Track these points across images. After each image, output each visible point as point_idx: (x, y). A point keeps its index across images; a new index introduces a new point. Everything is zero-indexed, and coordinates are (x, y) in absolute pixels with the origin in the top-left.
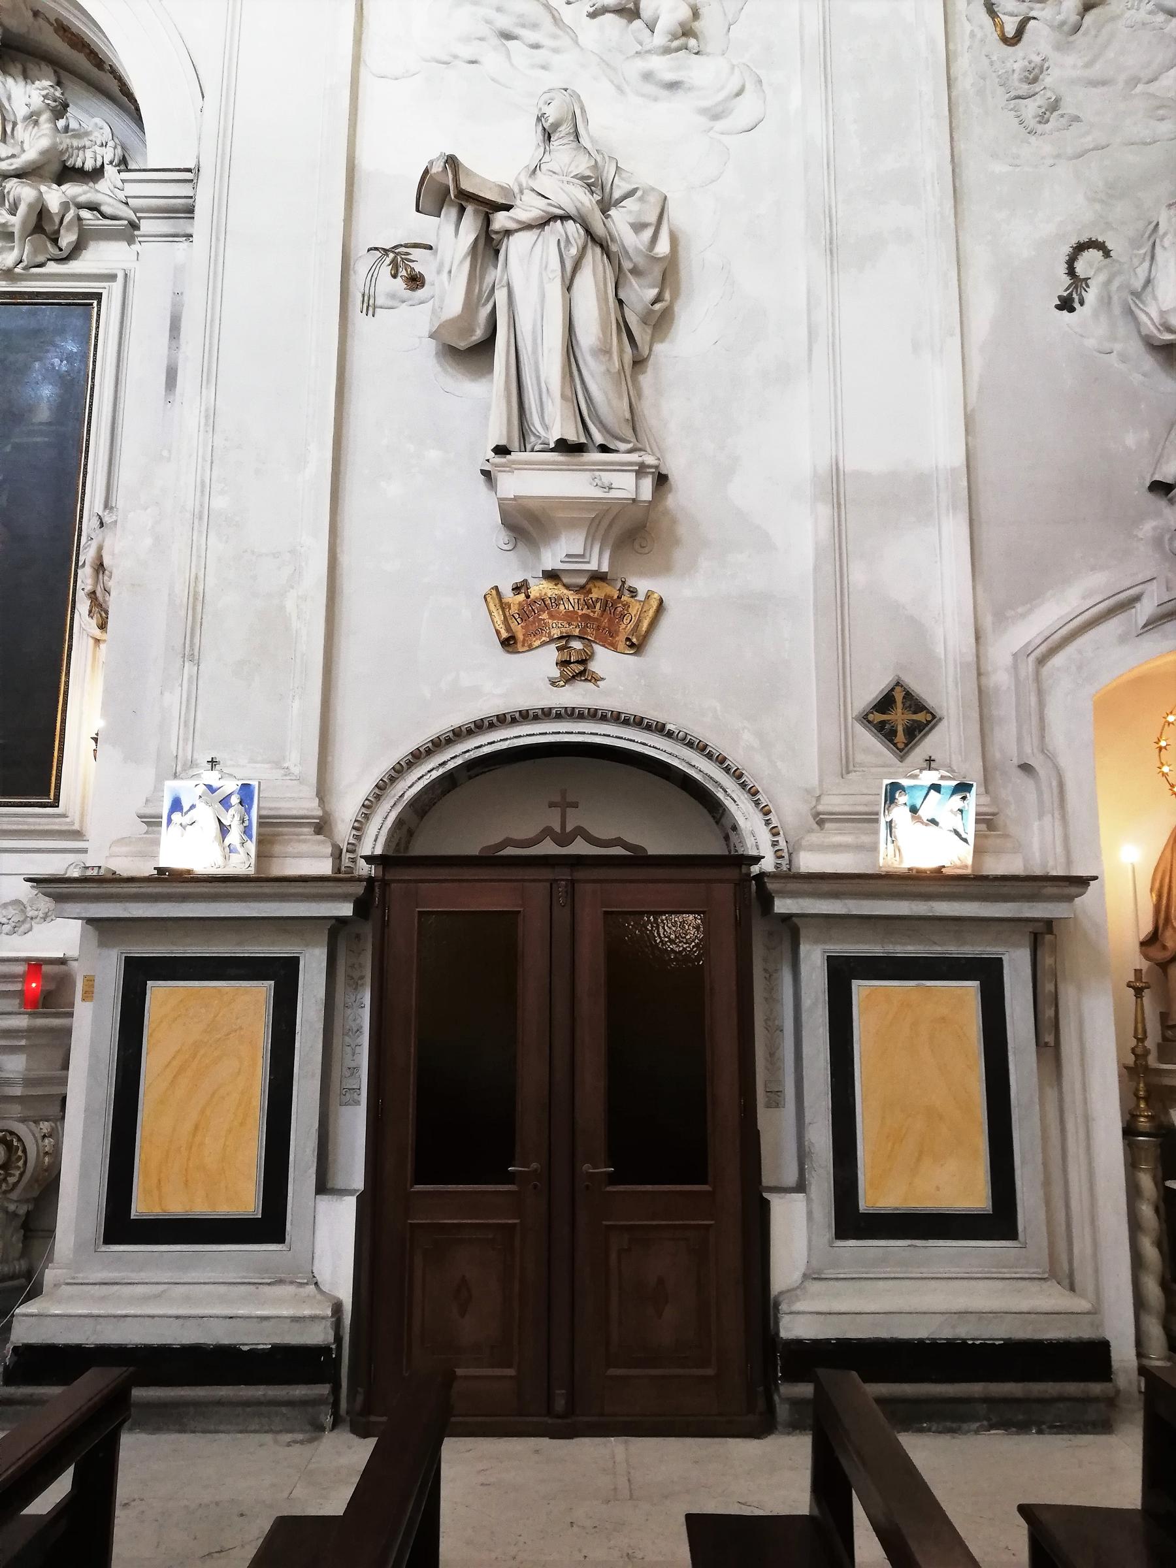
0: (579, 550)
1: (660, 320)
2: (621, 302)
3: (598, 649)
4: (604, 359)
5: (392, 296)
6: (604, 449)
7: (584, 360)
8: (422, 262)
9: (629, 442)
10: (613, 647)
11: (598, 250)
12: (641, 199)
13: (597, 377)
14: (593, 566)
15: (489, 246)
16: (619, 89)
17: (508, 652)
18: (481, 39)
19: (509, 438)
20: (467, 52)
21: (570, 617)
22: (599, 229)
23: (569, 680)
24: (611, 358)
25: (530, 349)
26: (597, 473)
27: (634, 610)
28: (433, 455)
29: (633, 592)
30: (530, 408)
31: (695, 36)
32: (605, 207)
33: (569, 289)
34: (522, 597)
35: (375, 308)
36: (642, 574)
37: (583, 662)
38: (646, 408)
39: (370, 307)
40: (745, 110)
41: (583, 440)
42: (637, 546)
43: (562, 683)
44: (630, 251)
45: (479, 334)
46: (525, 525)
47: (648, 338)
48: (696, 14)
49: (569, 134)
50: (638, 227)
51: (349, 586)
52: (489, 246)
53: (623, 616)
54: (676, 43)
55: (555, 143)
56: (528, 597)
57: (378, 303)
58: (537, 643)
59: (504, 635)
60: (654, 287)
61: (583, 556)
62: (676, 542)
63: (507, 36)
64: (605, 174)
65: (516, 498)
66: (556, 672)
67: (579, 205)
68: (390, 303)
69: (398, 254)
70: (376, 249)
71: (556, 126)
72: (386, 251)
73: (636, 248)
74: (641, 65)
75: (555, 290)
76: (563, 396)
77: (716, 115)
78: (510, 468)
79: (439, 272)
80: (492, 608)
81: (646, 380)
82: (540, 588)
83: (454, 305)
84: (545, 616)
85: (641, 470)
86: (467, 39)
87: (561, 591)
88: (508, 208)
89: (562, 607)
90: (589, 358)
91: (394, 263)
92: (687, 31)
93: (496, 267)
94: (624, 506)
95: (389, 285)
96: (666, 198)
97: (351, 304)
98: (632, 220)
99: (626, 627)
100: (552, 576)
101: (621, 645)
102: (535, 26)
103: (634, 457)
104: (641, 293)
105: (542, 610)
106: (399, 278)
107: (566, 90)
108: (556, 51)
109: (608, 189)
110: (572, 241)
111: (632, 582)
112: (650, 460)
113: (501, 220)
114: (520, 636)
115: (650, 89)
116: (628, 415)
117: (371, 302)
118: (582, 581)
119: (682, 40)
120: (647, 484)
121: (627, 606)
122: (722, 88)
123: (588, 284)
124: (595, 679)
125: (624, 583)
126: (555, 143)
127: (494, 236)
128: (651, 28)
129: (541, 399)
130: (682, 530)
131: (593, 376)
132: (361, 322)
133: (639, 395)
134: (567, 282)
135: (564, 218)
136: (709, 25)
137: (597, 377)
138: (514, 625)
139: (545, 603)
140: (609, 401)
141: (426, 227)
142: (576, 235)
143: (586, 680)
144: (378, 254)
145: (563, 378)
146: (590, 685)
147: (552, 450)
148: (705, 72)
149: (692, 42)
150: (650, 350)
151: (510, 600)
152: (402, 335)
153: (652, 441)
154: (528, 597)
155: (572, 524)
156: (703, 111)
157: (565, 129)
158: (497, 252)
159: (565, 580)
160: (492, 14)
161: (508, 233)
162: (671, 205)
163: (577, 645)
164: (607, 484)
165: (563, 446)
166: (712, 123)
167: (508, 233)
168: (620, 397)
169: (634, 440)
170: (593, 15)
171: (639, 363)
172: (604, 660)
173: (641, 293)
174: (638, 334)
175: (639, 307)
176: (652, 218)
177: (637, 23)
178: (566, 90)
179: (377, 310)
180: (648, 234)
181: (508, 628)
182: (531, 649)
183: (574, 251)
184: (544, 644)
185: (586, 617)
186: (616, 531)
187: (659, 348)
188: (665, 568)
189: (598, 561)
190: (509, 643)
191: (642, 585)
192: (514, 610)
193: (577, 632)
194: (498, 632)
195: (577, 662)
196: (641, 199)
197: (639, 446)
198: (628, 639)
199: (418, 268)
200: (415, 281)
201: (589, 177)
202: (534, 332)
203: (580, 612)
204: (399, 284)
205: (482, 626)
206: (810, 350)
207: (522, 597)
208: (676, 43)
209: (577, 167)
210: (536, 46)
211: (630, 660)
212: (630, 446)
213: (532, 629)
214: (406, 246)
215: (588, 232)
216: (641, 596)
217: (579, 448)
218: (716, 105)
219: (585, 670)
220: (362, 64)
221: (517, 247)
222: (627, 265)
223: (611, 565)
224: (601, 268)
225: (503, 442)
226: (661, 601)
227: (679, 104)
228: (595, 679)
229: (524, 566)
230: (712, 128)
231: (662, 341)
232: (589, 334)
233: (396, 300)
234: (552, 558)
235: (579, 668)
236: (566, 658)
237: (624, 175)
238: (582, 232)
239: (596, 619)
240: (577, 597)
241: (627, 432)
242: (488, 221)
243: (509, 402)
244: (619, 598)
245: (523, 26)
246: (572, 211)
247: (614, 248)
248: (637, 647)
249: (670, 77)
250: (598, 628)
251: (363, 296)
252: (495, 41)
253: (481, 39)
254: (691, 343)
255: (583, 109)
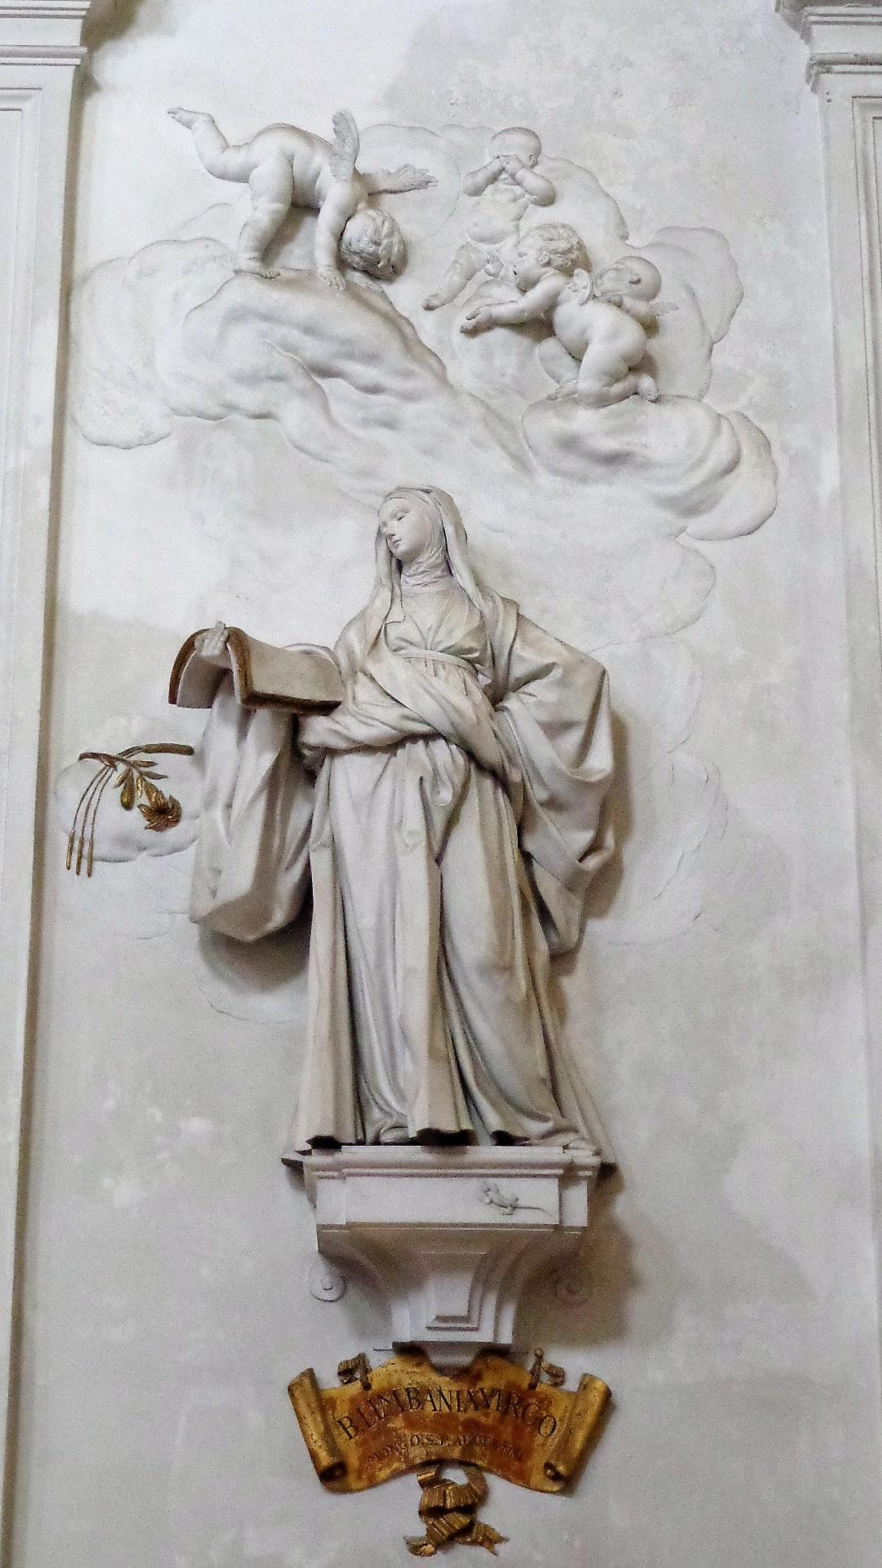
0: (459, 1307)
1: (598, 886)
2: (526, 857)
3: (497, 1485)
4: (500, 979)
5: (124, 841)
6: (503, 1139)
7: (468, 985)
8: (176, 780)
9: (546, 1119)
10: (521, 1477)
11: (488, 783)
12: (563, 683)
13: (487, 1010)
14: (485, 1336)
15: (299, 767)
16: (520, 462)
17: (333, 1490)
18: (279, 378)
19: (338, 1123)
20: (249, 398)
21: (443, 1425)
22: (491, 752)
23: (443, 1542)
24: (513, 975)
25: (371, 958)
26: (491, 1180)
27: (558, 1411)
28: (197, 1125)
29: (558, 1376)
30: (372, 1060)
31: (653, 373)
32: (496, 697)
33: (438, 860)
34: (356, 1387)
35: (91, 860)
36: (572, 1339)
37: (469, 1509)
38: (575, 1037)
39: (84, 857)
40: (743, 496)
41: (466, 1125)
42: (563, 1292)
43: (430, 1548)
44: (543, 772)
45: (279, 917)
46: (366, 1265)
47: (576, 915)
48: (650, 327)
49: (435, 567)
50: (555, 729)
51: (43, 1374)
52: (299, 767)
53: (538, 1422)
54: (618, 388)
55: (412, 581)
56: (367, 1386)
57: (97, 852)
58: (383, 1474)
59: (326, 1460)
60: (583, 827)
61: (467, 1319)
62: (630, 1280)
63: (326, 373)
64: (498, 633)
65: (350, 1226)
66: (418, 1529)
67: (457, 719)
68: (119, 852)
69: (133, 765)
70: (95, 756)
71: (413, 554)
72: (111, 761)
73: (554, 768)
74: (554, 423)
75: (415, 867)
76: (432, 1050)
77: (690, 506)
78: (342, 1172)
79: (208, 804)
80: (302, 1403)
81: (573, 986)
82: (384, 1367)
83: (240, 878)
84: (398, 1423)
85: (568, 1175)
86: (252, 379)
87: (423, 1377)
88: (327, 708)
89: (429, 1407)
90: (474, 978)
91: (126, 780)
92: (640, 365)
93: (311, 799)
94: (542, 1236)
95: (118, 820)
96: (604, 672)
97: (56, 853)
98: (544, 717)
99: (544, 1446)
100: (411, 1351)
101: (537, 1477)
102: (371, 358)
103: (552, 1153)
104: (562, 840)
105: (391, 1414)
106: (136, 811)
107: (427, 492)
108: (409, 397)
109: (502, 662)
110: (445, 777)
111: (556, 1357)
112: (584, 1156)
113: (317, 731)
114: (353, 1461)
115: (572, 463)
116: (542, 1070)
117: (86, 851)
118: (465, 1360)
119: (632, 379)
120: (578, 1196)
121: (545, 1402)
122: (701, 461)
123: (469, 851)
124: (490, 1540)
125: (540, 1358)
126: (409, 581)
127: (306, 752)
128: (577, 356)
129: (391, 1048)
130: (643, 1261)
131: (483, 1011)
132: (65, 882)
133: (562, 1013)
134: (436, 849)
135: (429, 737)
136: (677, 344)
137: (487, 1010)
138: (342, 1440)
139: (398, 1400)
140: (510, 1054)
141: (190, 724)
142: (451, 768)
143: (474, 1543)
144: (98, 765)
145: (432, 1017)
146: (482, 1552)
147: (412, 1142)
148: (669, 433)
149: (646, 382)
150: (582, 931)
151: (333, 1393)
152: (144, 905)
153: (589, 1109)
154: (367, 1386)
155: (450, 1265)
156: (668, 503)
157: (430, 557)
158: (311, 777)
159: (436, 1359)
160: (295, 336)
161: (330, 752)
162: (613, 682)
163: (457, 1476)
164: (508, 1201)
165: (431, 1138)
166: (682, 522)
167: (330, 752)
168: (529, 1040)
169: (553, 1113)
170: (472, 332)
171: (562, 958)
172: (507, 1504)
173: (562, 840)
174: (552, 918)
175: (562, 866)
176: (581, 713)
177: (549, 346)
178: (427, 492)
179: (97, 865)
180: (575, 737)
181: (333, 1450)
182: (373, 1483)
183: (446, 796)
184: (397, 1474)
185: (471, 1426)
186: (524, 1272)
187: (594, 926)
188: (609, 1328)
189: (496, 1325)
190: (333, 1476)
191: (574, 1363)
192: (343, 1411)
193: (456, 1453)
194: (314, 1456)
195: (458, 1509)
196: (563, 683)
197: (564, 1123)
198: (548, 1466)
199: (167, 789)
200: (164, 814)
201: (471, 650)
202: (379, 931)
203: (462, 1417)
204: (135, 819)
205: (282, 1442)
206: (864, 938)
207: (356, 1387)
208: (618, 388)
209: (450, 633)
210: (375, 390)
211: (553, 1504)
212: (549, 1125)
213: (374, 1446)
214: (149, 750)
215: (471, 755)
216: (571, 1385)
217: (462, 1139)
218: (695, 490)
219: (472, 1524)
220: (68, 419)
221: (348, 777)
222: (538, 794)
223: (516, 1332)
224: (492, 818)
225: (327, 1132)
226: (608, 1394)
227: (625, 489)
228: (490, 1540)
229: (362, 1331)
230: (683, 530)
231: (602, 913)
232: (473, 942)
233: (128, 848)
234: (413, 1319)
235: (464, 1520)
236: (436, 1502)
237: (533, 634)
238: (461, 760)
239: (493, 1429)
240: (455, 1387)
241: (544, 1100)
242: (295, 729)
243: (336, 1054)
244: (532, 1386)
245: (350, 356)
246: (444, 726)
247: (515, 776)
248: (566, 1480)
249: (609, 445)
250: (495, 1444)
251: (72, 840)
252: (301, 382)
253: (279, 378)
254: (664, 895)
255: (458, 525)
